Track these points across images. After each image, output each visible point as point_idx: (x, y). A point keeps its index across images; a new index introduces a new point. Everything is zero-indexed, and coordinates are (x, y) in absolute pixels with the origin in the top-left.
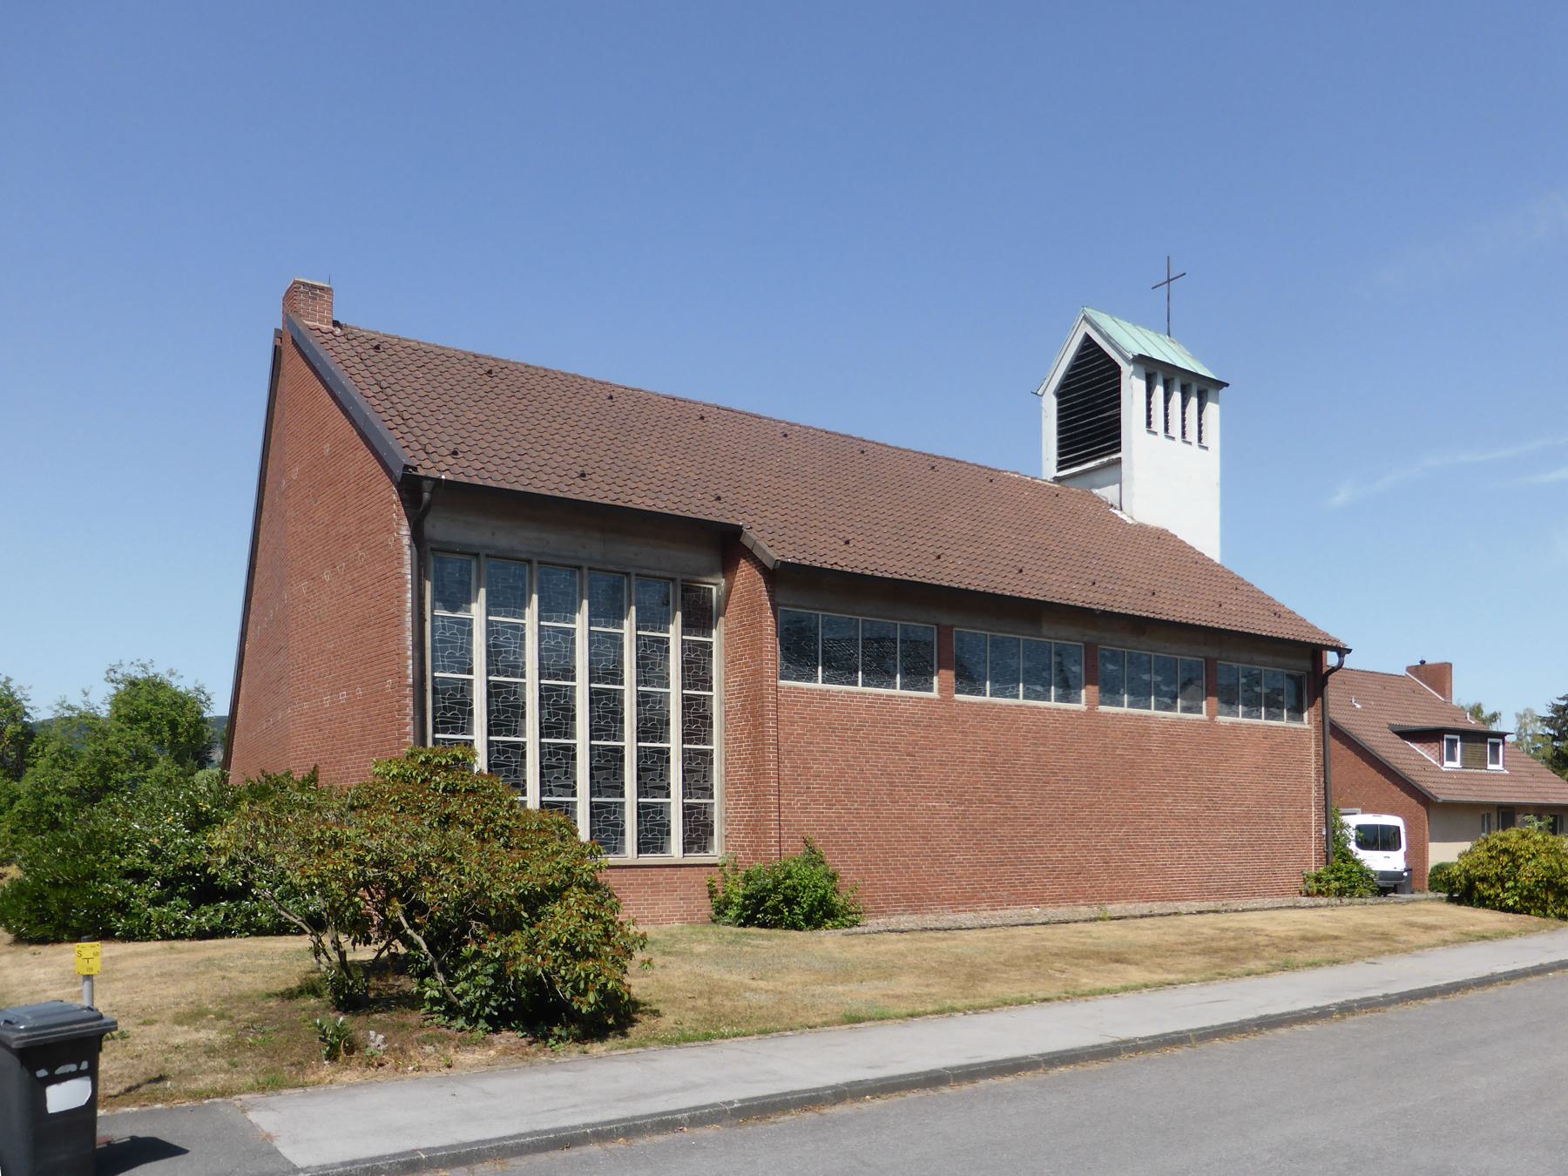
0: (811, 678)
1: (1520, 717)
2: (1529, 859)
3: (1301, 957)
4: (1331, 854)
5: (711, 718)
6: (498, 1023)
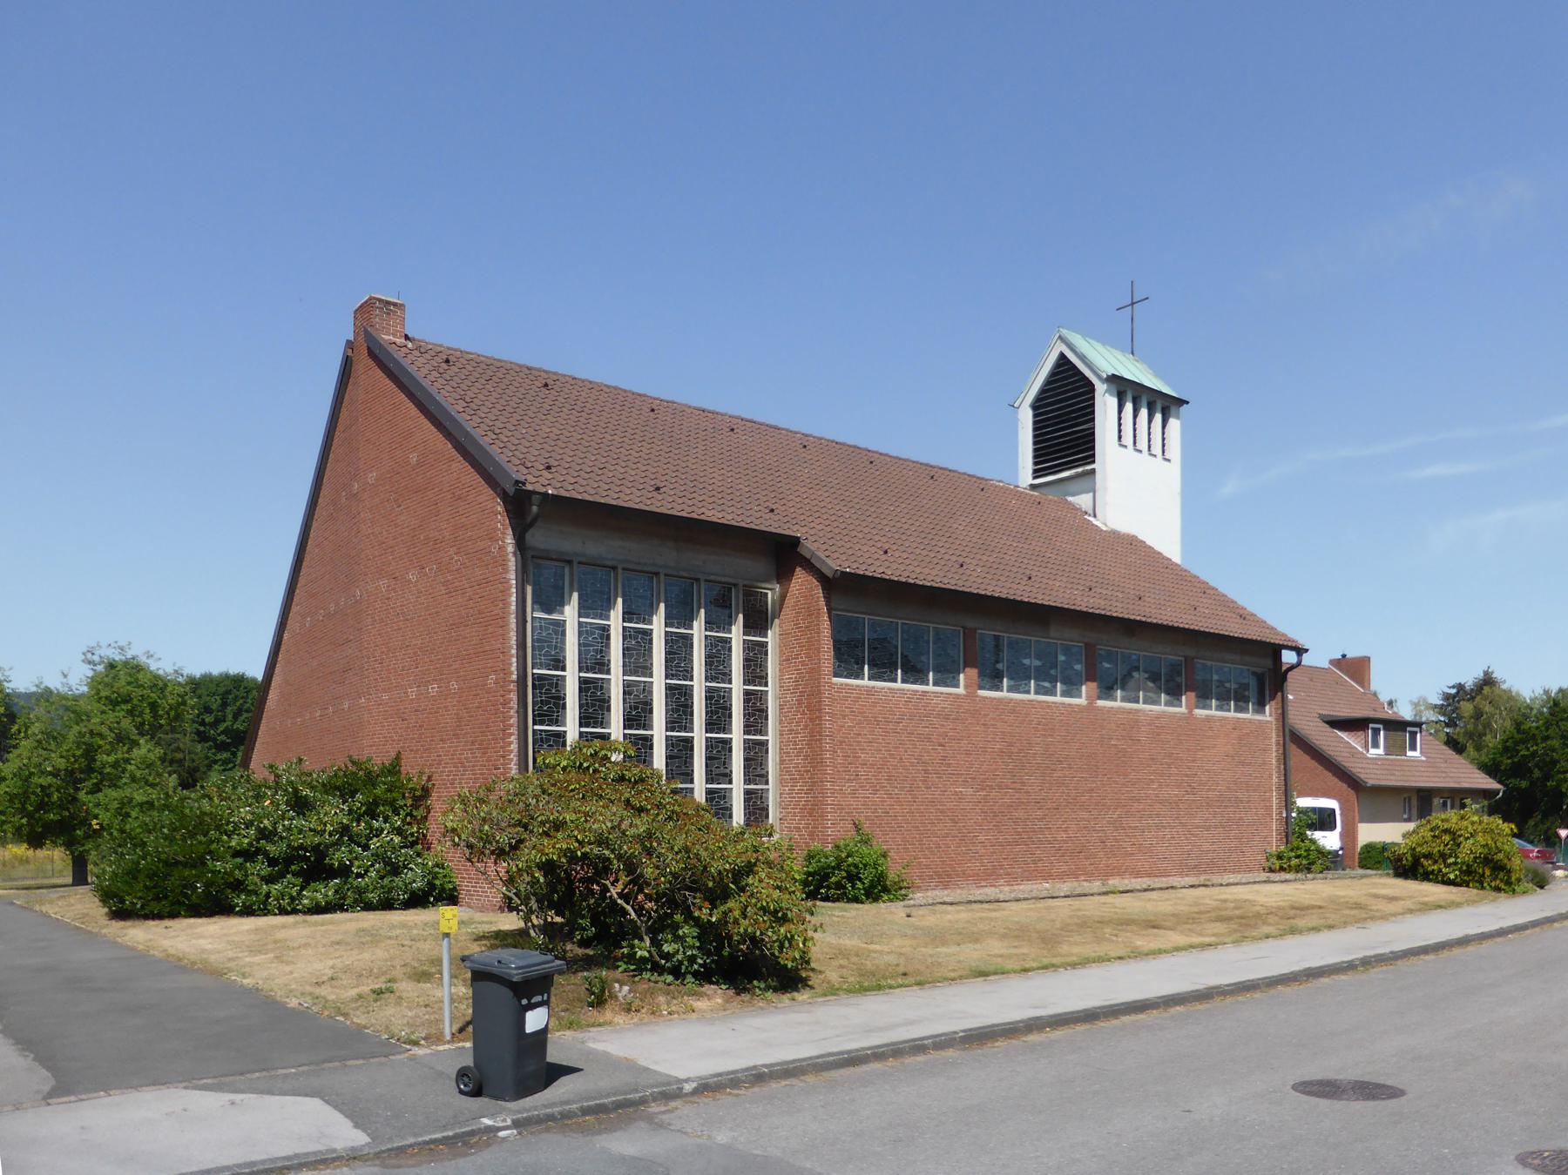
0: (859, 676)
1: (1416, 705)
2: (1468, 838)
3: (1301, 923)
4: (1290, 833)
5: (767, 711)
6: (705, 976)
